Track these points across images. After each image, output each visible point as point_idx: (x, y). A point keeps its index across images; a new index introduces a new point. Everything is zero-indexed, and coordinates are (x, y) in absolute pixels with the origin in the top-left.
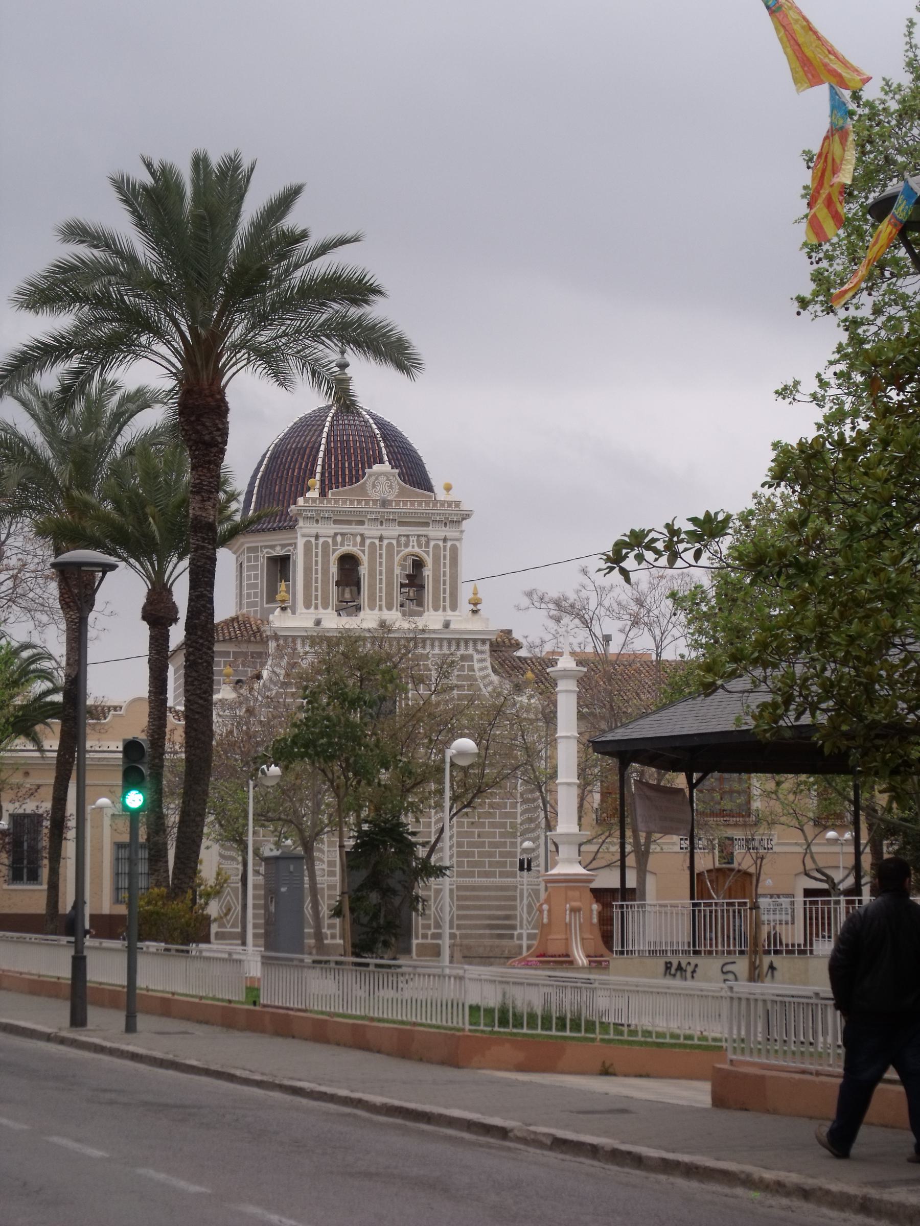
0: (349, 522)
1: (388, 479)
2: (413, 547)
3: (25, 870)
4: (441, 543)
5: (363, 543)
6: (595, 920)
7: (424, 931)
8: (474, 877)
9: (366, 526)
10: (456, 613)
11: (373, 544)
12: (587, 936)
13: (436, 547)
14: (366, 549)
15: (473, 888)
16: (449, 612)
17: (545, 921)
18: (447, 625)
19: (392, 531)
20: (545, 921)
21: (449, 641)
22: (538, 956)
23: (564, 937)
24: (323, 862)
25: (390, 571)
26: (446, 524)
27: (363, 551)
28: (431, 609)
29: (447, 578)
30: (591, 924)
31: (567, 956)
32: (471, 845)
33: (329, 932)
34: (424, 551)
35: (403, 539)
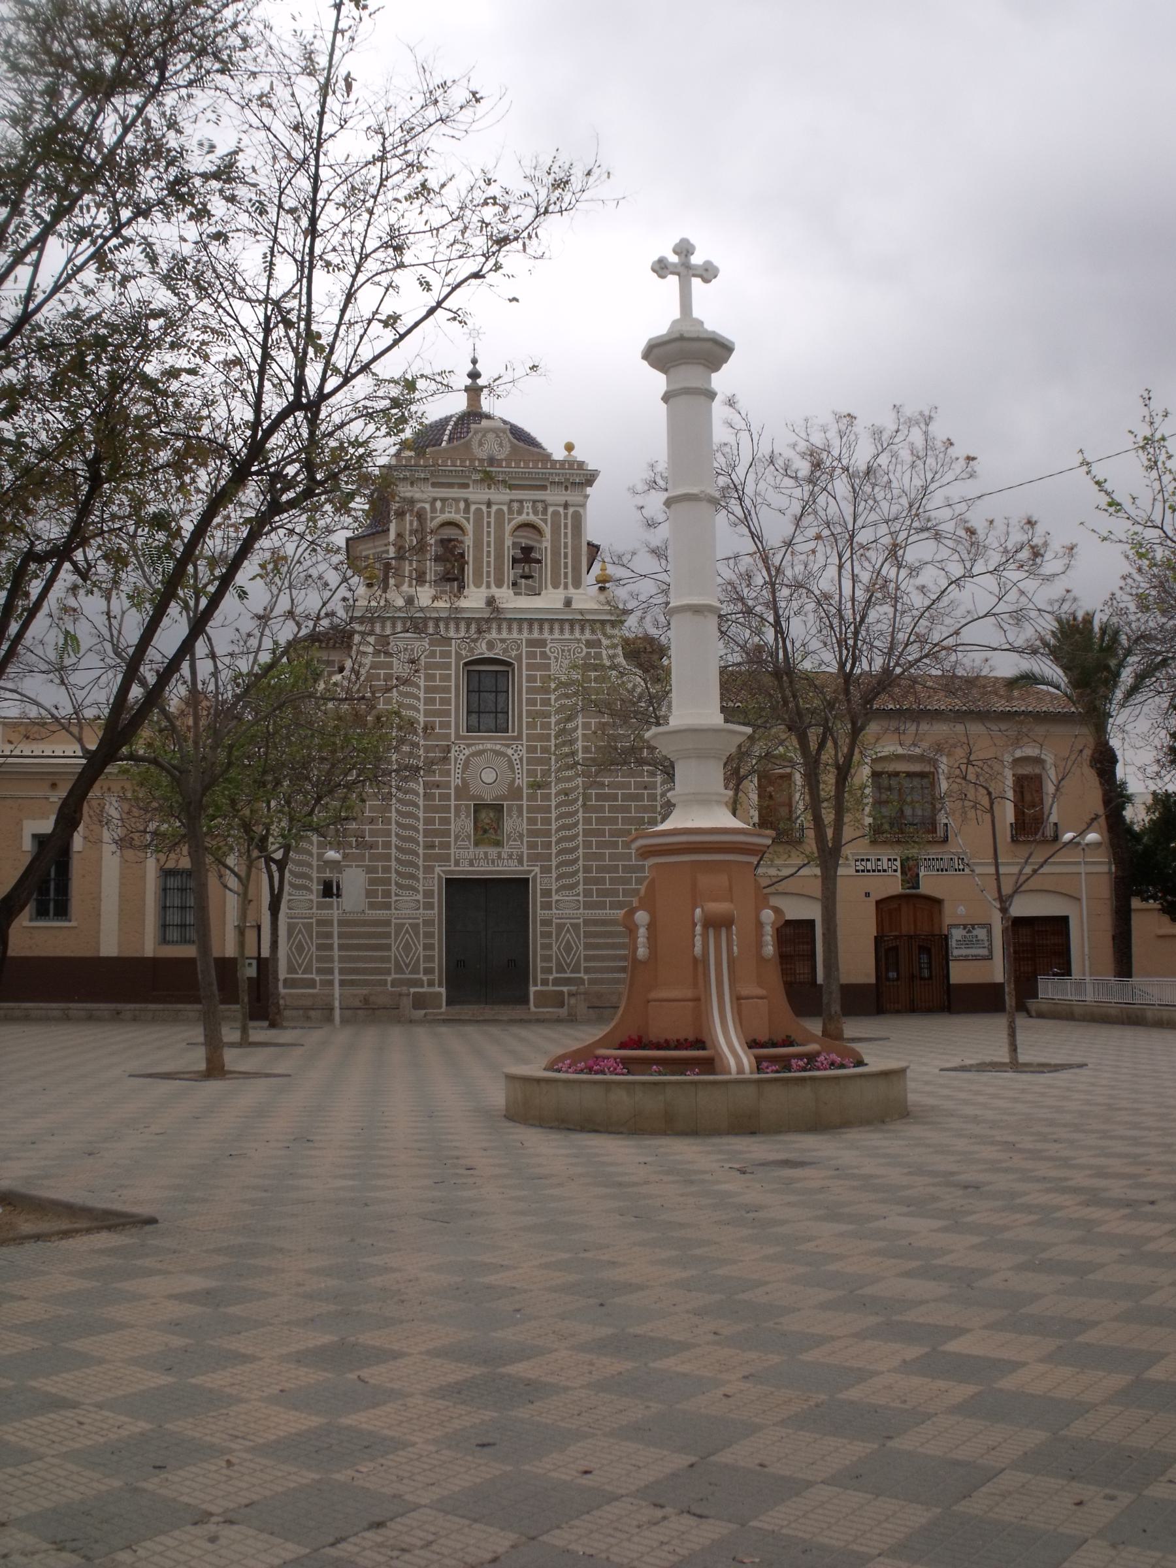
0: (450, 485)
1: (498, 436)
2: (528, 514)
3: (52, 905)
4: (561, 510)
5: (467, 510)
6: (769, 950)
7: (544, 976)
8: (605, 908)
9: (471, 489)
10: (580, 591)
11: (479, 510)
12: (749, 989)
14: (471, 516)
15: (604, 923)
16: (572, 590)
17: (642, 952)
18: (568, 603)
19: (501, 496)
20: (642, 952)
21: (572, 623)
22: (623, 1046)
23: (689, 993)
24: (418, 892)
27: (468, 519)
28: (549, 586)
29: (569, 550)
30: (761, 959)
31: (700, 1044)
32: (600, 869)
33: (425, 978)
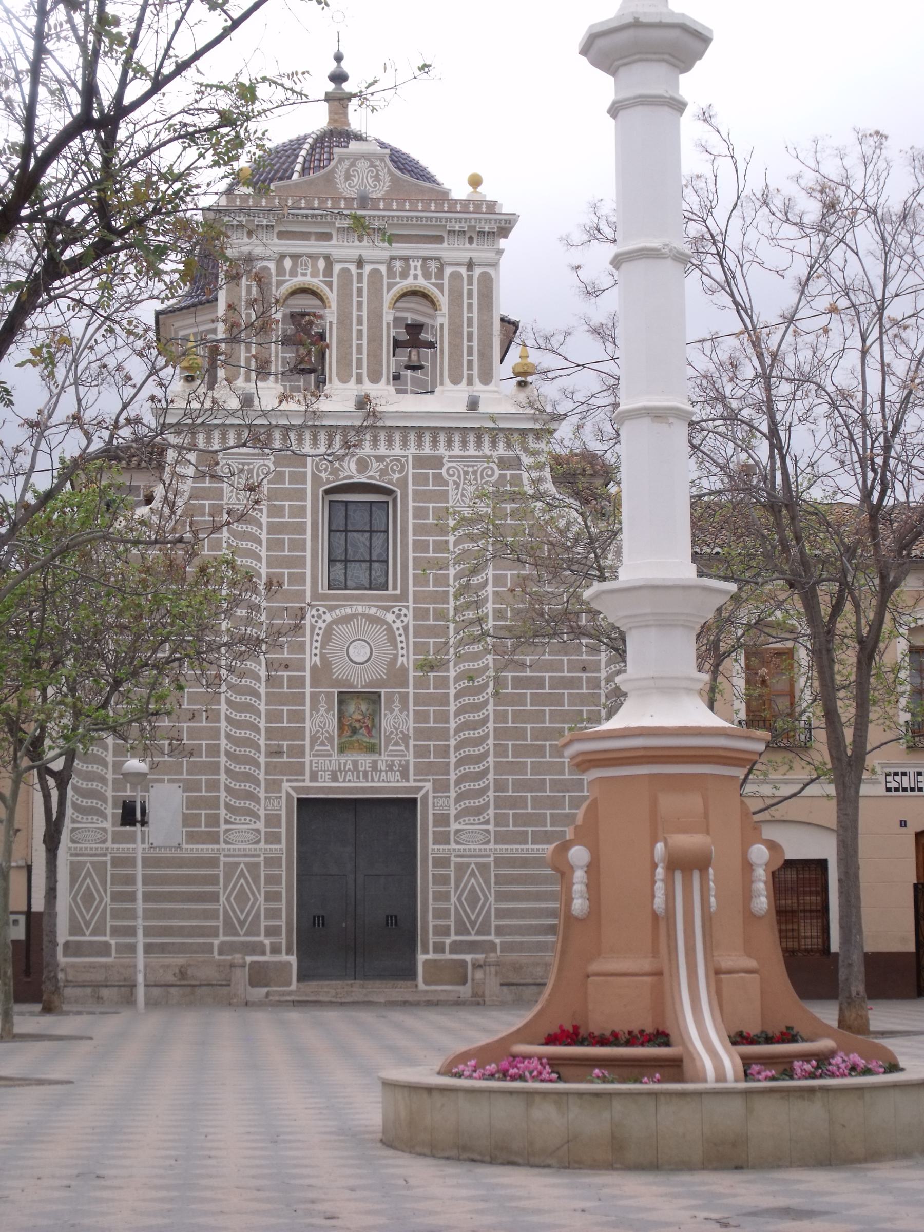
1: (372, 165)
2: (416, 277)
4: (463, 271)
7: (438, 939)
8: (526, 843)
9: (334, 242)
13: (456, 276)
14: (335, 279)
15: (525, 862)
16: (478, 386)
17: (579, 905)
18: (473, 404)
20: (579, 905)
22: (551, 1040)
23: (646, 965)
24: (258, 817)
25: (376, 316)
26: (471, 239)
28: (447, 380)
30: (750, 916)
31: (661, 1037)
33: (267, 942)
34: (433, 284)
35: (398, 265)
